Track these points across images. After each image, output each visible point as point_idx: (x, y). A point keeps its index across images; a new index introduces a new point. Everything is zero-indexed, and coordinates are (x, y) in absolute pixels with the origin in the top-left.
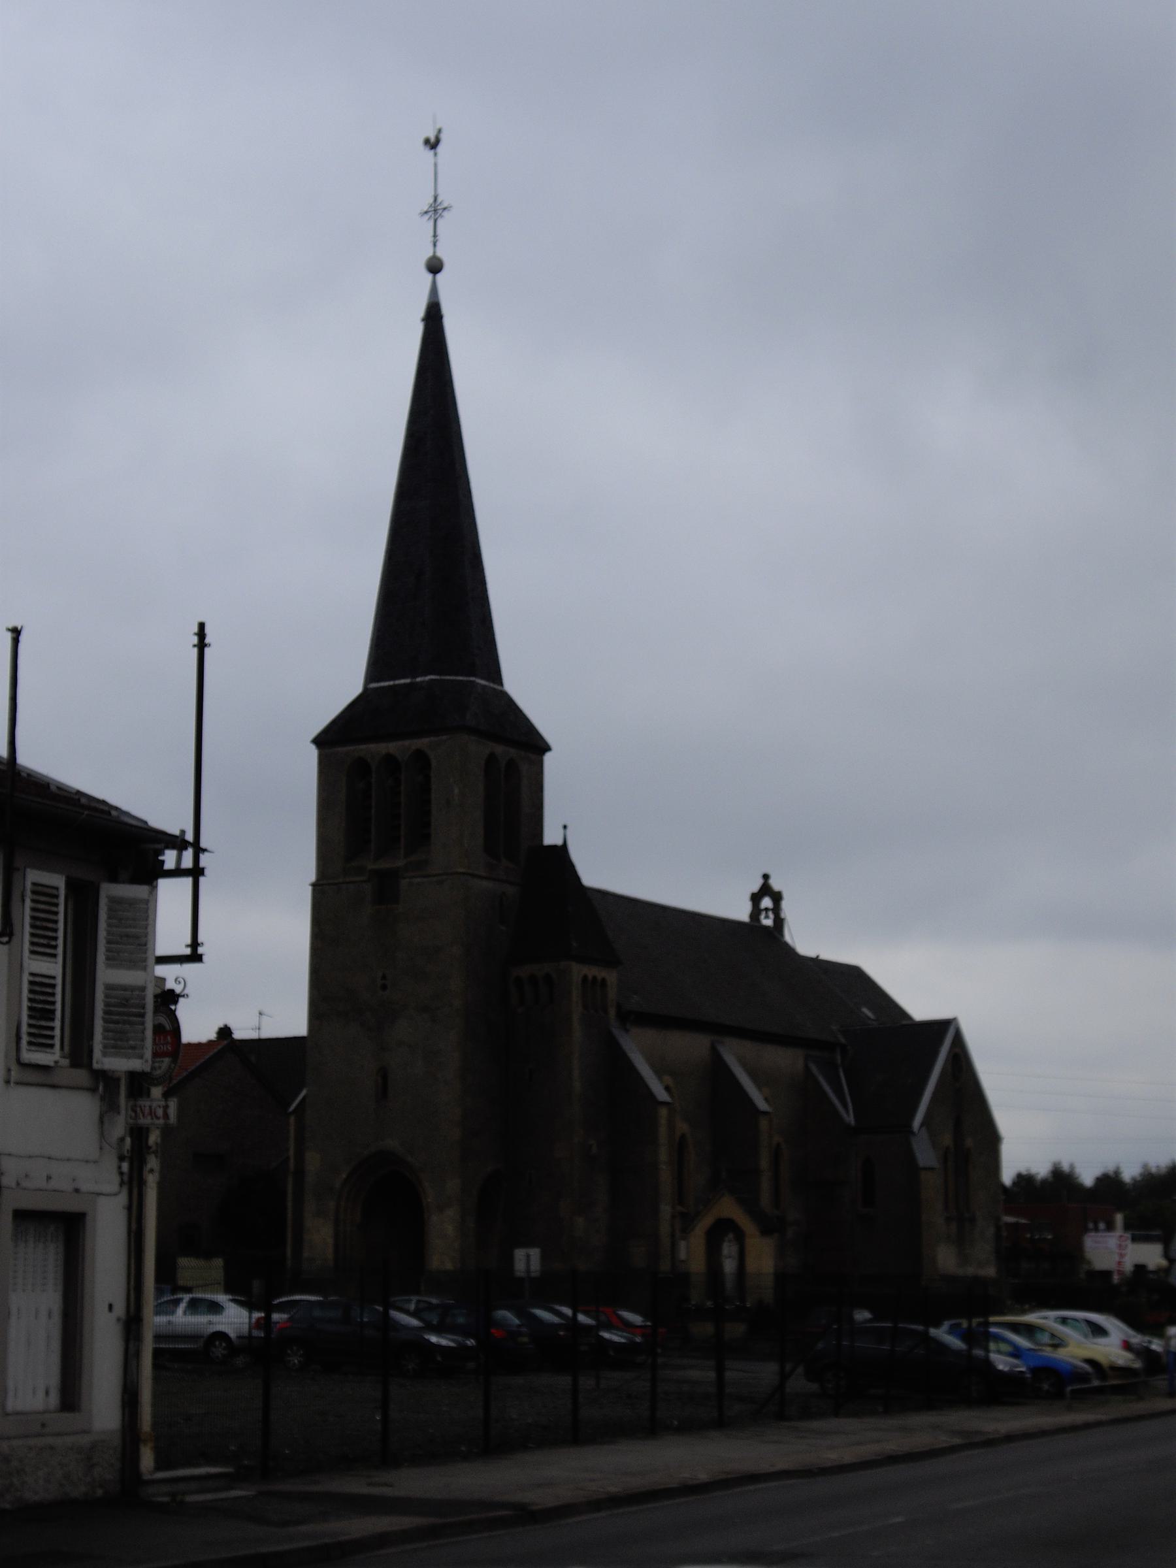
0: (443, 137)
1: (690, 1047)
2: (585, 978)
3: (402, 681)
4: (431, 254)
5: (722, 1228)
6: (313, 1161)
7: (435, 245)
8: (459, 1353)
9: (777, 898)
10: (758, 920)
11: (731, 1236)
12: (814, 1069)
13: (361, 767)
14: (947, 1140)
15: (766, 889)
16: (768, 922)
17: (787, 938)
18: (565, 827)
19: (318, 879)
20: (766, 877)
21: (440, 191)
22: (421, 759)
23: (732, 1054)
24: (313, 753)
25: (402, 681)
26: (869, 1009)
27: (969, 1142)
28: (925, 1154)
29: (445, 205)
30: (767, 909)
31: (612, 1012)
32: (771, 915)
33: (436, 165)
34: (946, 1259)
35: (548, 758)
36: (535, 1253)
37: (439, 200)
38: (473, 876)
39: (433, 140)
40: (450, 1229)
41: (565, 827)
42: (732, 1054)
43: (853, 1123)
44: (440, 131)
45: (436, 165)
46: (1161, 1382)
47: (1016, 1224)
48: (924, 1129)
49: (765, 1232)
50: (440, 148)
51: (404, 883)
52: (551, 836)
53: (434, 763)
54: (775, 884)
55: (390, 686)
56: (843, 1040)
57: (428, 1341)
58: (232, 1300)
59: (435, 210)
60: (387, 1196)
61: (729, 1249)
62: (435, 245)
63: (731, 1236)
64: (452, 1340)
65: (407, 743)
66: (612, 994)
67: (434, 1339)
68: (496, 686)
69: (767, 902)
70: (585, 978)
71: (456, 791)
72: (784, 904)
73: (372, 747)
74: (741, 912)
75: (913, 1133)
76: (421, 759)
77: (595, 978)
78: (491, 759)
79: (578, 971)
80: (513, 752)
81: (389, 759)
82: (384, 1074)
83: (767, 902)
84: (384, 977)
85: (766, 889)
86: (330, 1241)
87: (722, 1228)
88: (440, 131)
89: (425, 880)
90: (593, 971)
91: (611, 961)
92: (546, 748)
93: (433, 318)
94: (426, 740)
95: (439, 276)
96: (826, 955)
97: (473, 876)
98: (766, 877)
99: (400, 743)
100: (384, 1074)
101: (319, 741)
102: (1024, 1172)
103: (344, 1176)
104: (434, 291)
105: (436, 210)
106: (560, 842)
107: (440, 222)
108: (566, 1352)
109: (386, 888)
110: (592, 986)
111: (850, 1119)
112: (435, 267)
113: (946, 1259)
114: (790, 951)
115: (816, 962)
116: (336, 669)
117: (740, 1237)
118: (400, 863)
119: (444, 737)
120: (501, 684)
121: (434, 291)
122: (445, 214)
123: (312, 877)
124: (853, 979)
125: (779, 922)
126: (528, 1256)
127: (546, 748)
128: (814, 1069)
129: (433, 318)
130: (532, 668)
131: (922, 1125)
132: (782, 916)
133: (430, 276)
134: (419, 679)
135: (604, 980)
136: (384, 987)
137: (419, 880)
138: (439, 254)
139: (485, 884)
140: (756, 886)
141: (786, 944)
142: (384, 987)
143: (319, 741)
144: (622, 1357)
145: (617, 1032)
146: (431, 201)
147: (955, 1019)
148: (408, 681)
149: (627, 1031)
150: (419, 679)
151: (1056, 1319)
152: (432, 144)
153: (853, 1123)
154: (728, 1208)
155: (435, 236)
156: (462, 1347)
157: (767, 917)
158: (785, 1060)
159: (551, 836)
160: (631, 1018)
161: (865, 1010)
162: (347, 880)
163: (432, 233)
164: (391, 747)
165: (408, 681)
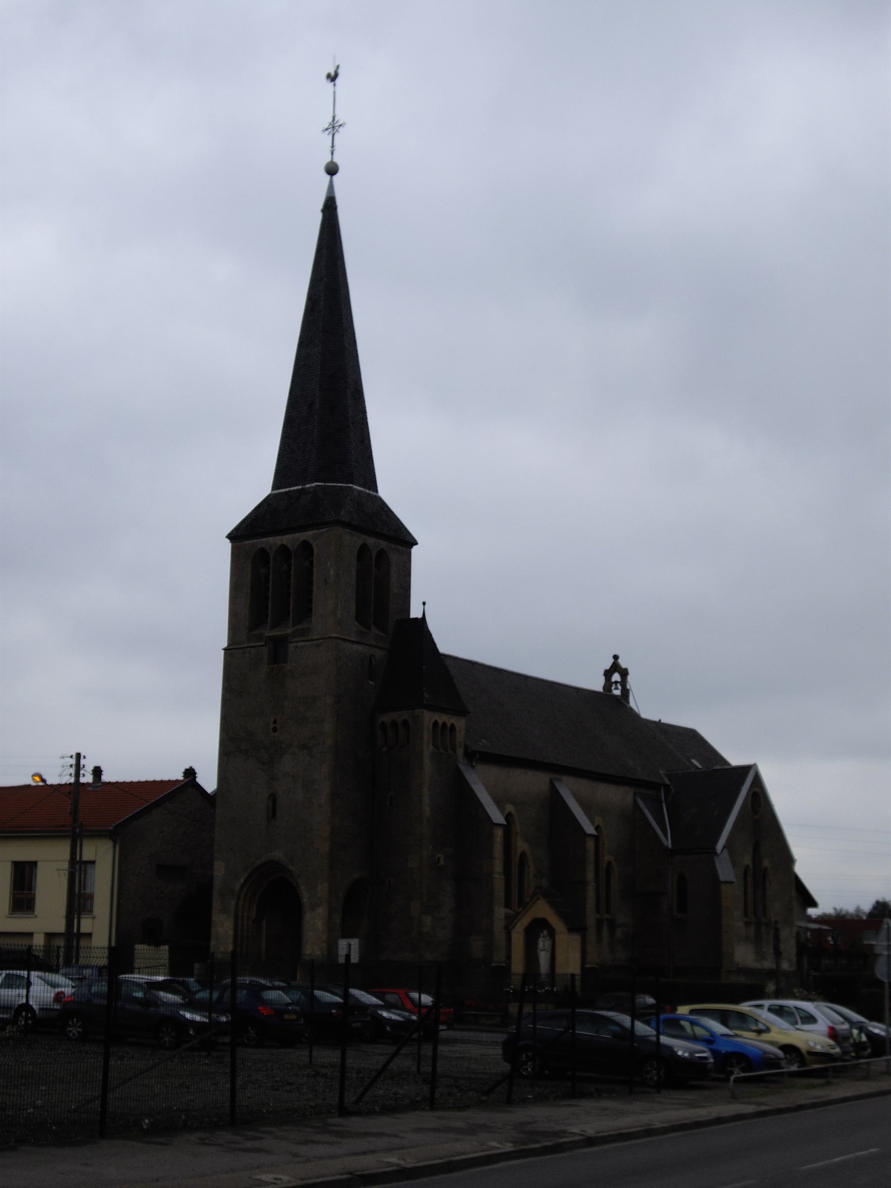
0: (340, 71)
1: (533, 782)
2: (436, 723)
3: (296, 488)
4: (329, 160)
5: (538, 927)
6: (219, 869)
7: (332, 154)
8: (406, 1025)
9: (624, 673)
10: (610, 691)
11: (545, 932)
12: (641, 803)
13: (262, 556)
14: (747, 860)
15: (615, 667)
16: (617, 692)
17: (632, 704)
18: (424, 603)
19: (229, 645)
20: (616, 657)
21: (336, 113)
22: (306, 547)
23: (567, 790)
24: (228, 545)
25: (296, 488)
26: (698, 761)
27: (766, 863)
28: (725, 871)
29: (341, 123)
30: (616, 682)
31: (460, 752)
32: (620, 687)
33: (334, 93)
34: (743, 955)
35: (415, 550)
36: (355, 943)
37: (336, 119)
38: (344, 640)
39: (333, 74)
40: (320, 925)
41: (424, 603)
42: (567, 790)
43: (670, 846)
44: (338, 67)
45: (334, 93)
46: (879, 1063)
47: (820, 929)
48: (725, 850)
49: (571, 930)
50: (338, 81)
51: (291, 646)
52: (415, 612)
53: (316, 551)
54: (623, 663)
55: (286, 492)
56: (668, 782)
57: (381, 1016)
58: (41, 978)
59: (333, 127)
60: (274, 894)
61: (543, 943)
62: (332, 154)
63: (545, 932)
64: (398, 1015)
65: (296, 535)
66: (460, 737)
67: (188, 1015)
68: (375, 494)
69: (616, 677)
70: (436, 723)
71: (332, 573)
72: (630, 678)
73: (271, 539)
74: (597, 684)
75: (716, 854)
76: (306, 547)
77: (444, 724)
78: (363, 550)
79: (429, 718)
80: (383, 544)
81: (283, 549)
82: (273, 798)
83: (616, 677)
84: (275, 722)
85: (615, 667)
86: (231, 933)
87: (538, 927)
88: (338, 67)
89: (307, 643)
90: (441, 718)
91: (461, 711)
92: (415, 543)
93: (330, 208)
94: (310, 533)
95: (335, 177)
96: (666, 720)
97: (344, 640)
98: (616, 657)
99: (291, 536)
100: (273, 798)
101: (231, 537)
102: (881, 900)
103: (242, 881)
104: (331, 187)
105: (334, 127)
106: (420, 616)
107: (336, 136)
108: (346, 1028)
109: (278, 651)
110: (442, 732)
111: (668, 843)
112: (332, 170)
113: (743, 955)
114: (635, 716)
115: (658, 725)
116: (252, 479)
117: (552, 933)
118: (289, 631)
119: (325, 530)
120: (377, 492)
121: (331, 187)
122: (341, 129)
123: (225, 645)
124: (691, 740)
125: (626, 692)
126: (350, 945)
127: (415, 543)
128: (641, 803)
129: (330, 208)
130: (398, 479)
131: (724, 847)
132: (628, 687)
133: (328, 177)
134: (307, 486)
135: (453, 726)
136: (275, 730)
137: (303, 643)
138: (336, 160)
139: (355, 647)
140: (608, 663)
141: (631, 709)
142: (275, 730)
143: (231, 537)
144: (398, 1035)
145: (463, 768)
146: (331, 120)
147: (755, 764)
148: (300, 487)
149: (473, 767)
150: (307, 486)
151: (770, 1010)
152: (332, 78)
153: (670, 846)
154: (542, 910)
155: (333, 147)
156: (213, 1024)
157: (616, 689)
158: (616, 796)
159: (415, 612)
160: (475, 757)
161: (694, 761)
162: (250, 645)
163: (330, 145)
164: (285, 539)
165: (300, 487)
